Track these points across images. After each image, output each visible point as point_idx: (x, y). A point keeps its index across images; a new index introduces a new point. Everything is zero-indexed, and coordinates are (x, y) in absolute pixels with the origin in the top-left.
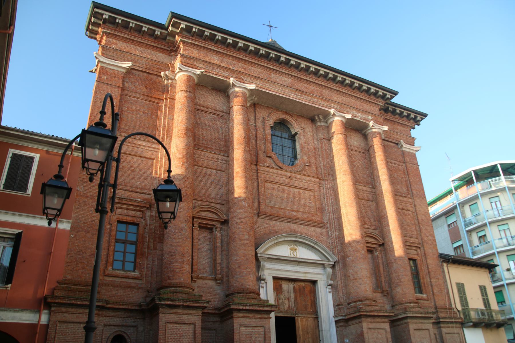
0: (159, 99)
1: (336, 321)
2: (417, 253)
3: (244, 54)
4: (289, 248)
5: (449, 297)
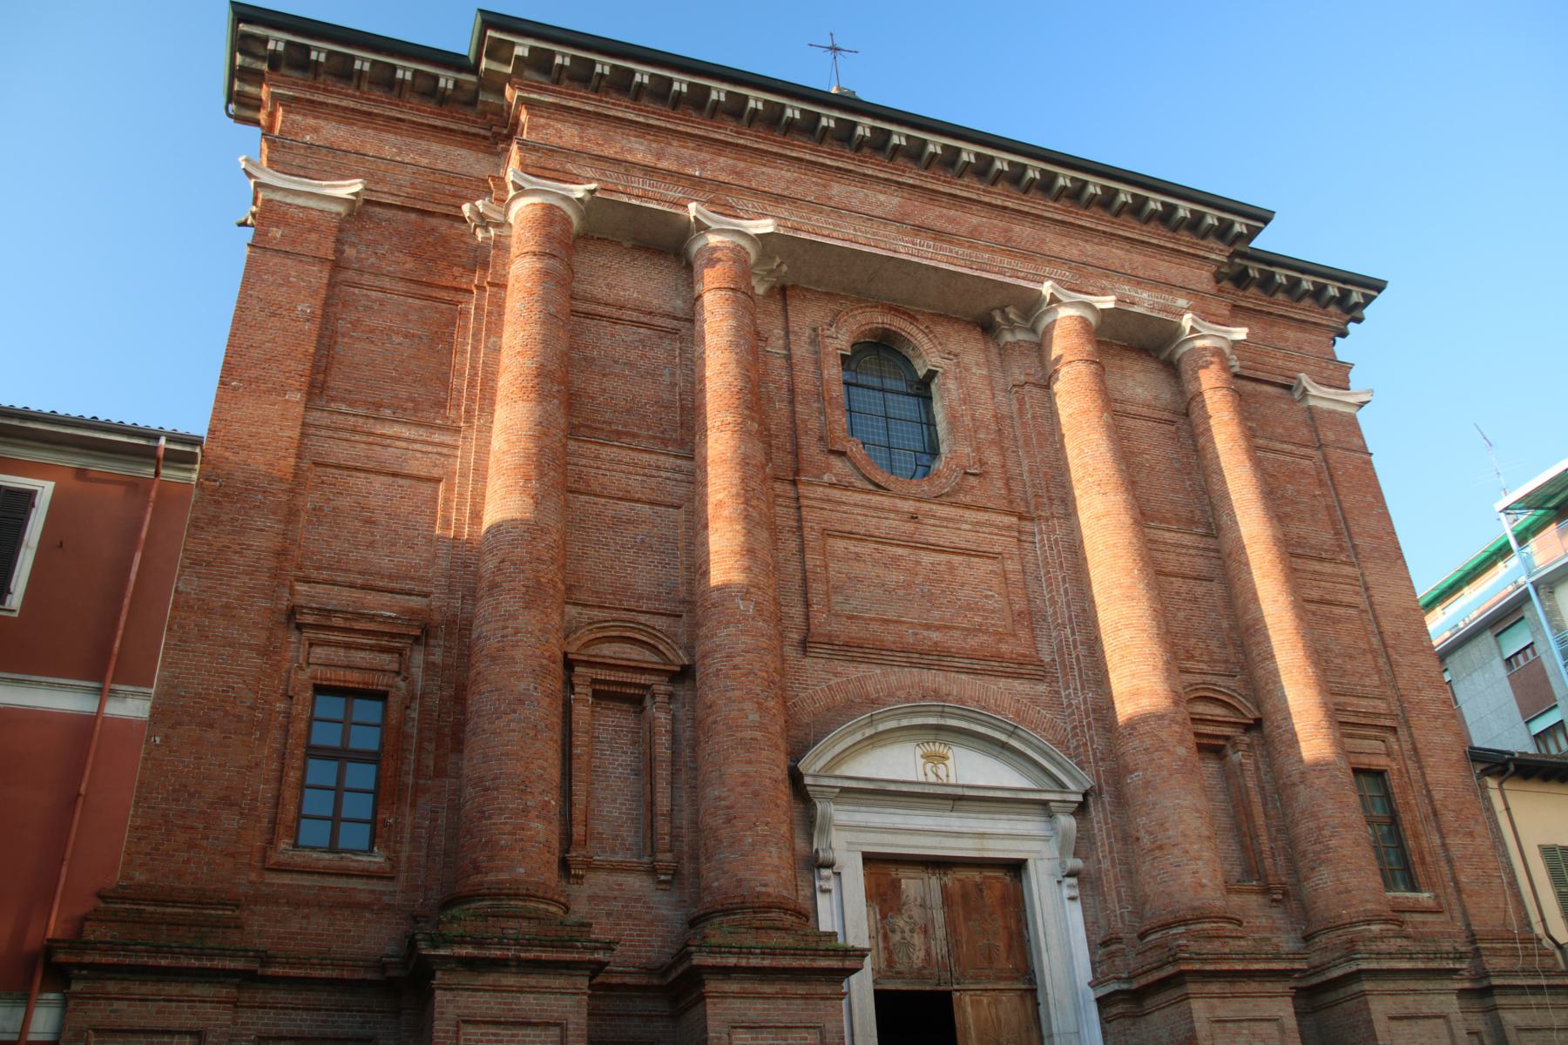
0: (456, 289)
1: (1099, 1000)
2: (1386, 747)
3: (731, 125)
4: (919, 752)
5: (1517, 895)
